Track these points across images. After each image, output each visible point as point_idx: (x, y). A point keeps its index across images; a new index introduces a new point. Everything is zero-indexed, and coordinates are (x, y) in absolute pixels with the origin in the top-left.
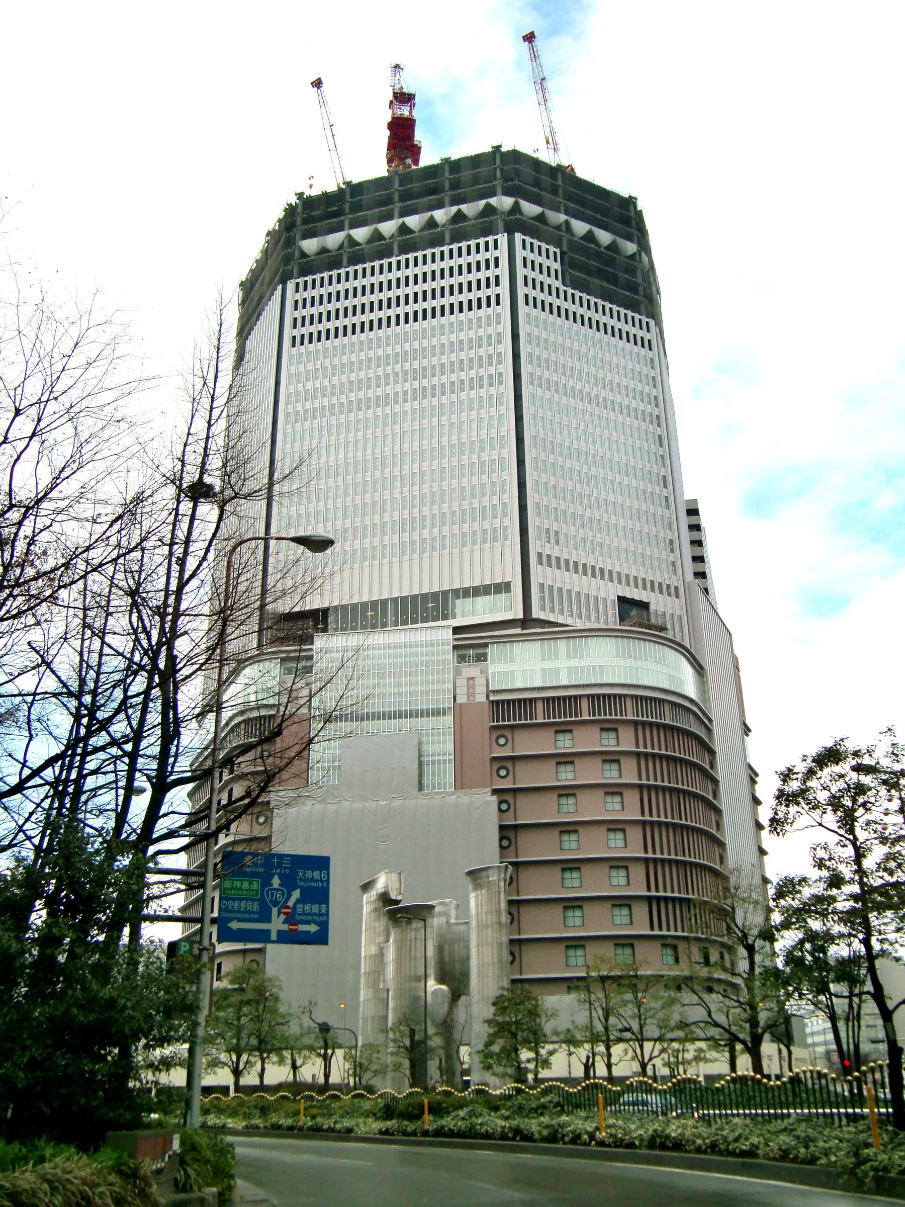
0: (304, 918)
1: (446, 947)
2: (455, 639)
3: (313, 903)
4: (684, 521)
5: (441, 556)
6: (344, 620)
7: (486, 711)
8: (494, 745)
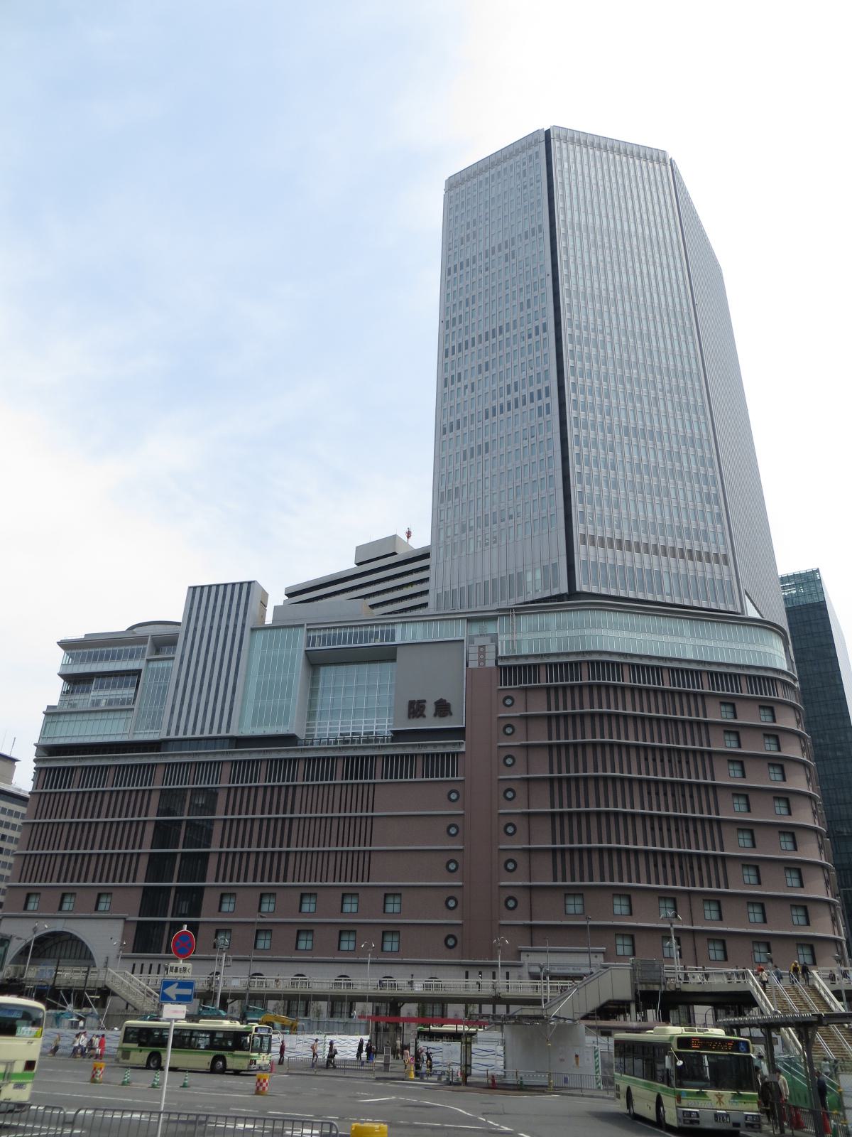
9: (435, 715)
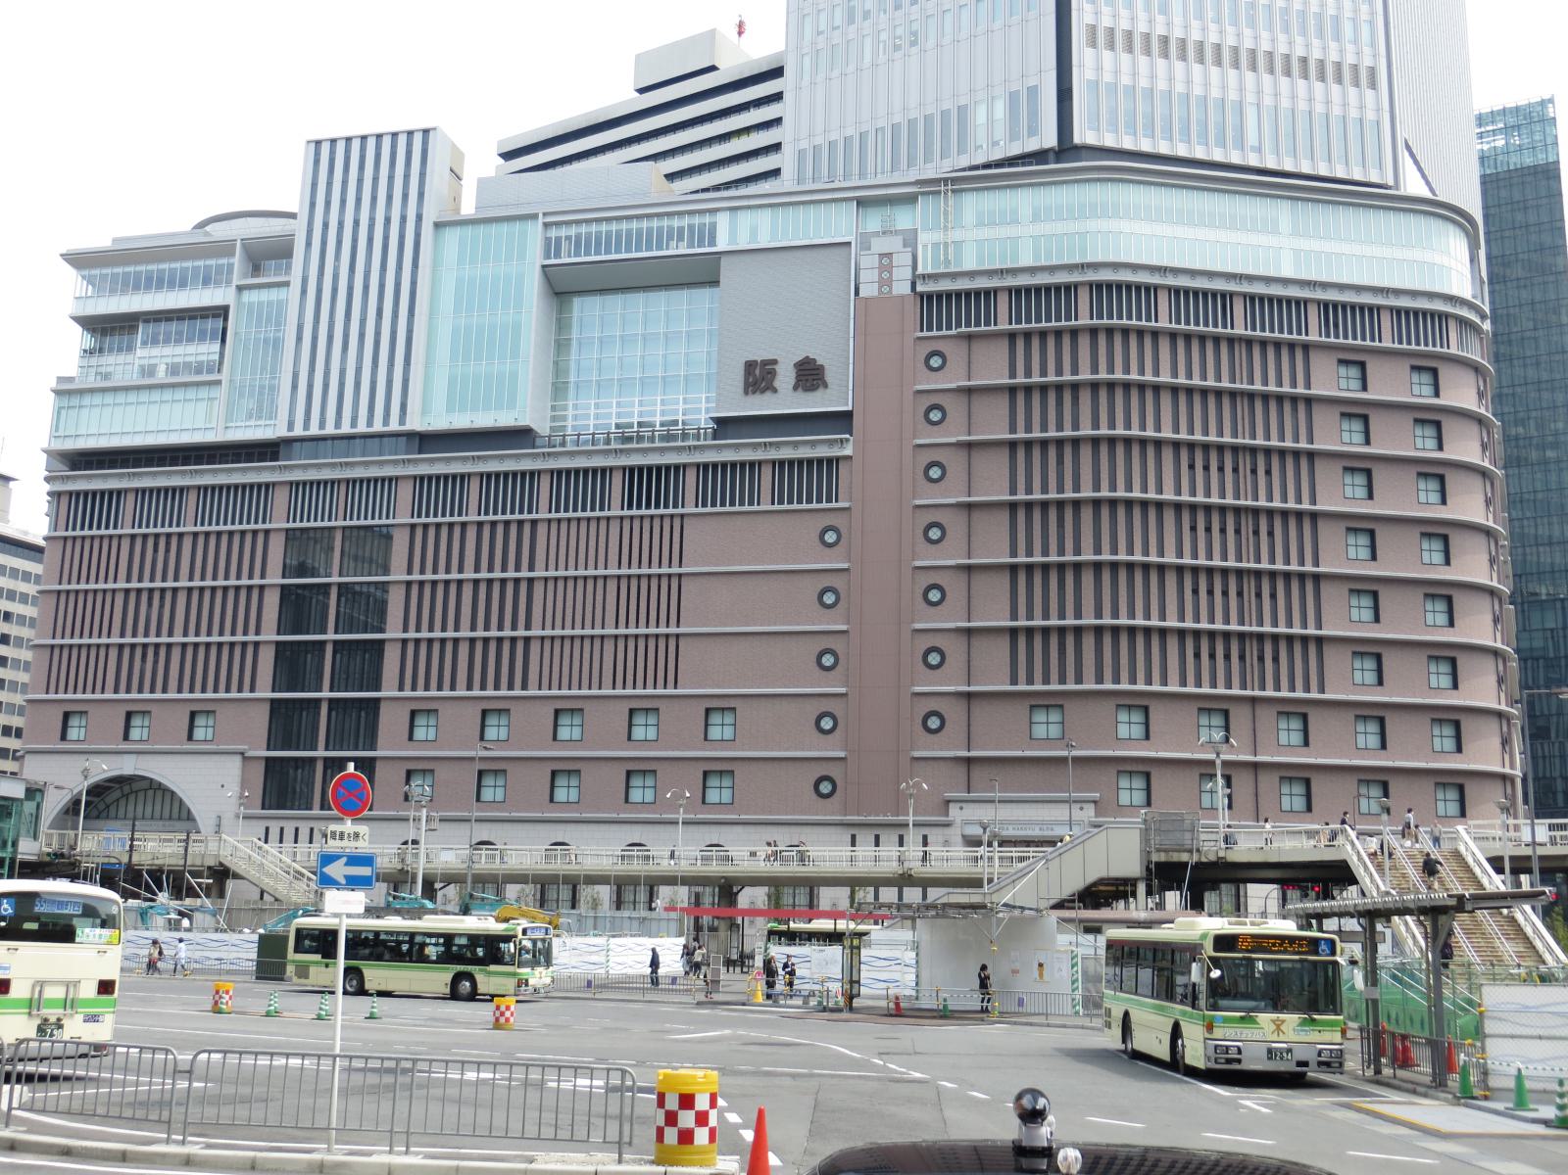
7: (912, 310)
9: (795, 388)
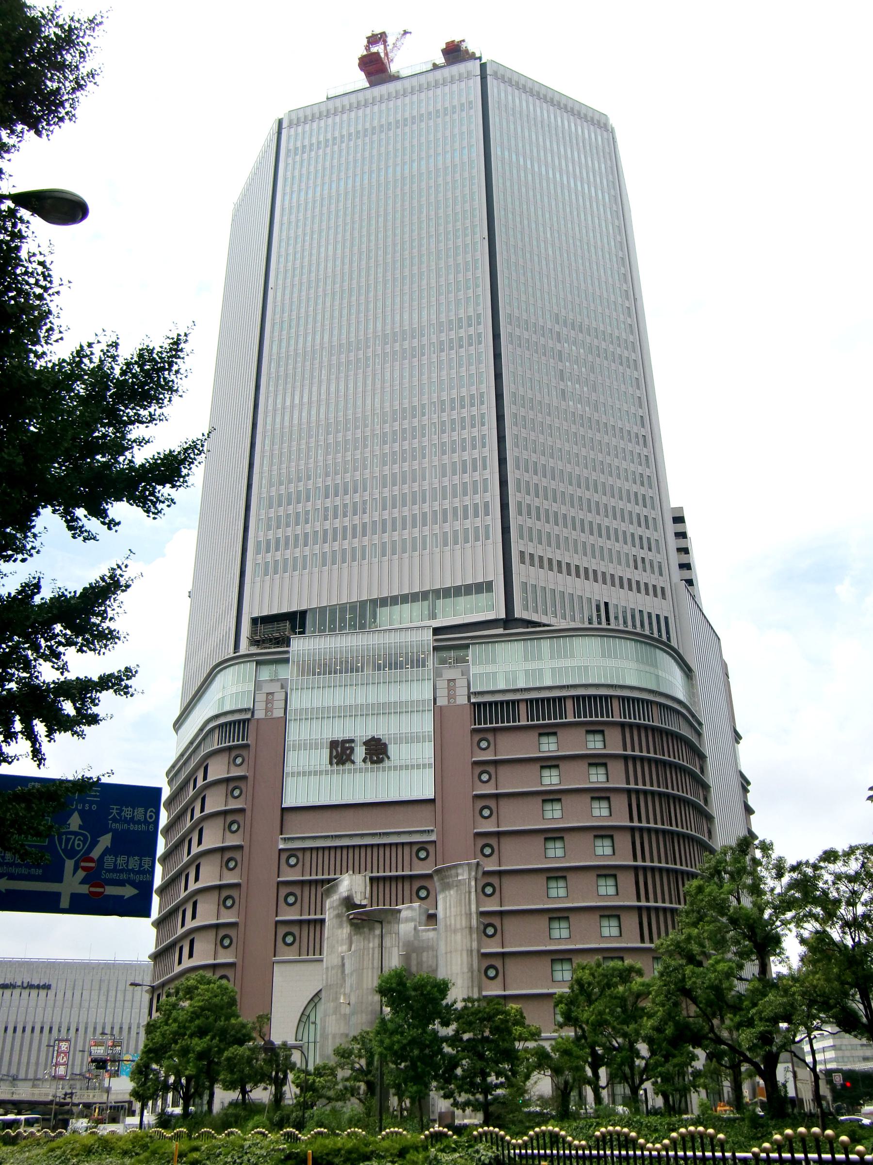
0: (114, 876)
1: (414, 955)
2: (436, 640)
3: (130, 854)
4: (671, 528)
5: (421, 556)
6: (323, 623)
7: (467, 714)
8: (476, 748)
